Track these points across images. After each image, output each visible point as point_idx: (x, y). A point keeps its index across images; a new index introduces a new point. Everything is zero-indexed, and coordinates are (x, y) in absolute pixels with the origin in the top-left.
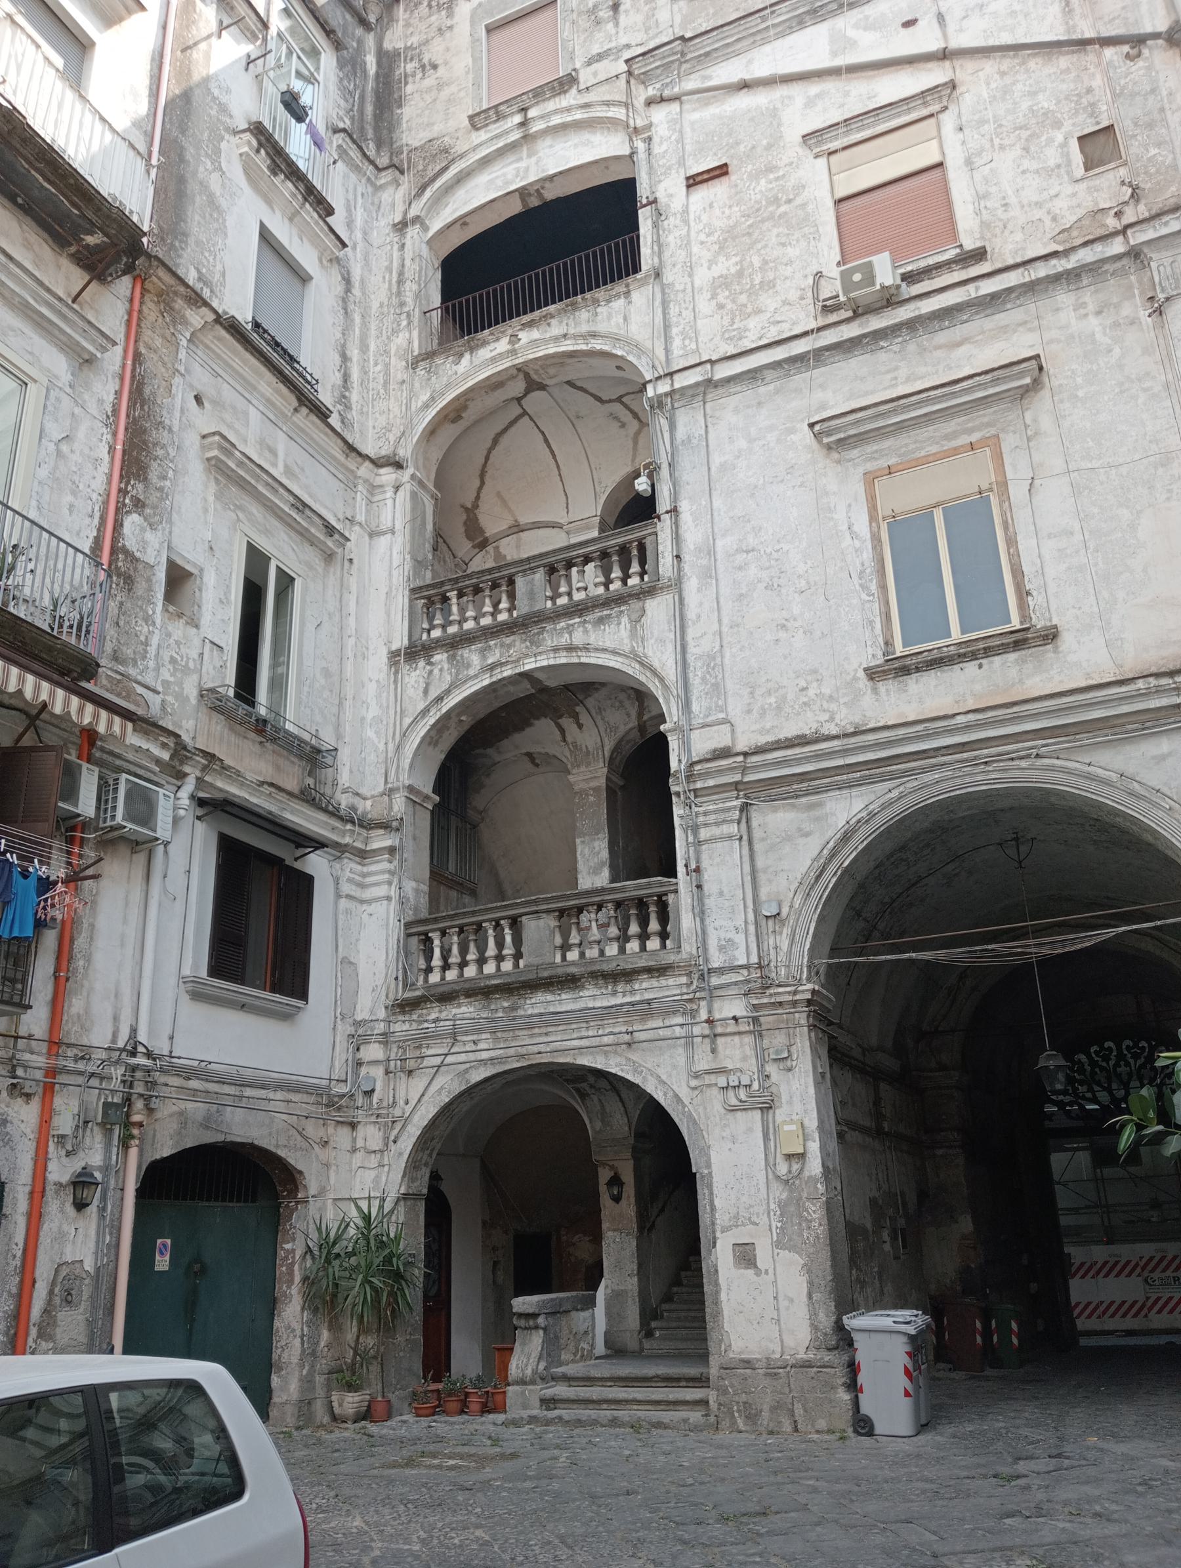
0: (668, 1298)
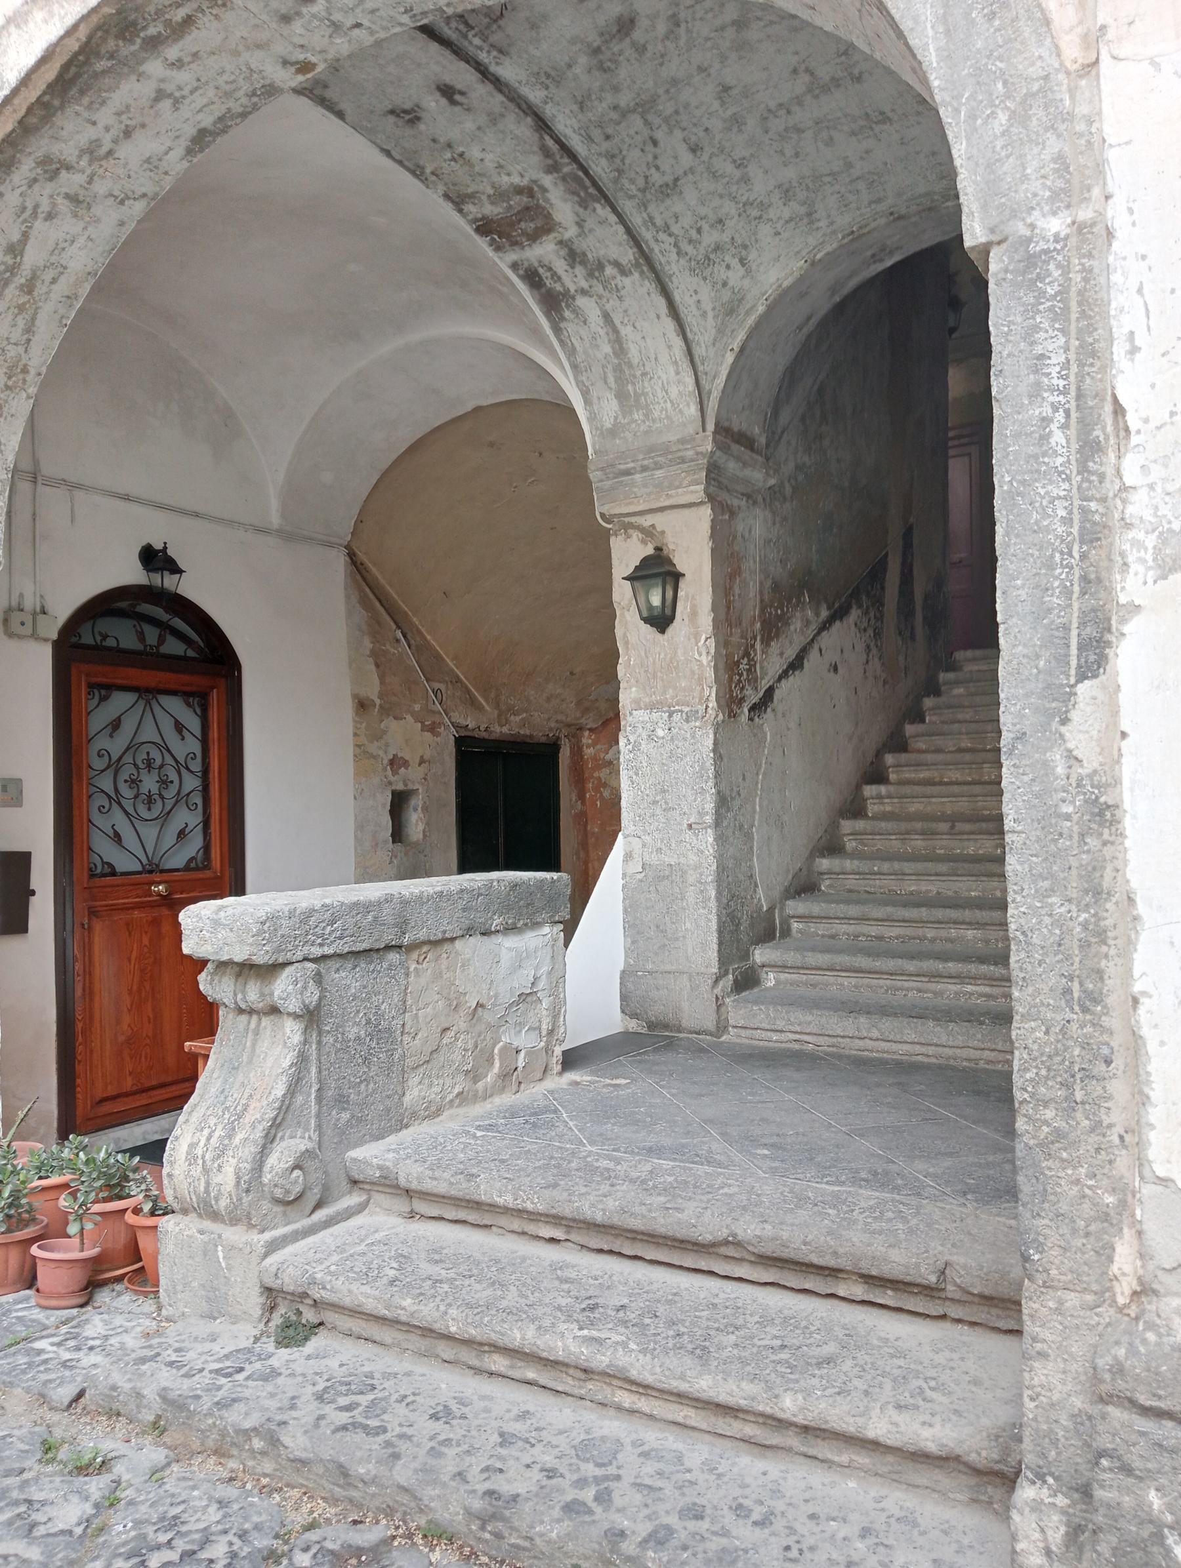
0: (804, 886)
